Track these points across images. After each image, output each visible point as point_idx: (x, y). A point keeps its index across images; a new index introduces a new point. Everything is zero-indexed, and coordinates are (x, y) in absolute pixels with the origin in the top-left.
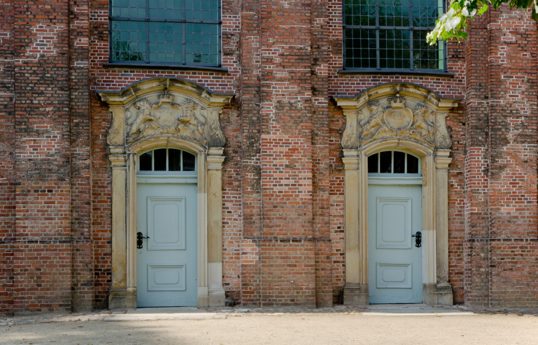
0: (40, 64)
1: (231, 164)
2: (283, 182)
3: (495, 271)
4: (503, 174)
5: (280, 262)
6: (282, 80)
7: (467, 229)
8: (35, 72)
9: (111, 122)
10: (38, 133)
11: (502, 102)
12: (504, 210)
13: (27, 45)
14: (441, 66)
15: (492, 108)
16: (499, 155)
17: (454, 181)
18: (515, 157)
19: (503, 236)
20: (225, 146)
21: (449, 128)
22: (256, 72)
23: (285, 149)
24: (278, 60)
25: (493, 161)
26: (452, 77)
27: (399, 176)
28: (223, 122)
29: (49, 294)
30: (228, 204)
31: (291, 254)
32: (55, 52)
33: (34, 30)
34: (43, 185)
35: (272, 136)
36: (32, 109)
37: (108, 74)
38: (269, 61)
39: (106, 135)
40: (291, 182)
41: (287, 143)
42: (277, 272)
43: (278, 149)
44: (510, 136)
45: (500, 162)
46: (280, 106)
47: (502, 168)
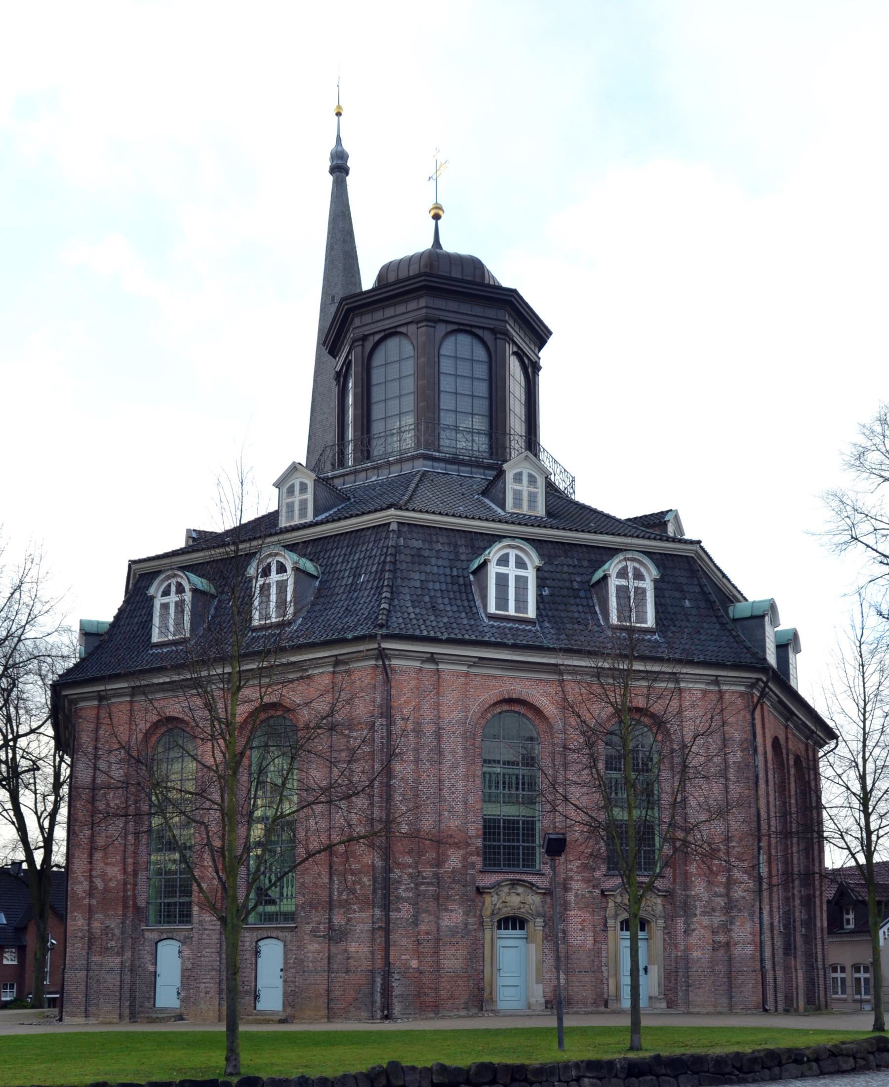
0: (453, 872)
1: (547, 927)
2: (579, 938)
3: (690, 989)
4: (694, 934)
5: (577, 984)
6: (578, 881)
7: (674, 965)
8: (450, 877)
9: (484, 903)
10: (451, 911)
11: (693, 893)
12: (695, 954)
13: (446, 861)
14: (537, 868)
15: (687, 896)
16: (692, 923)
17: (666, 937)
18: (700, 924)
19: (694, 970)
20: (544, 916)
21: (663, 906)
22: (563, 876)
23: (579, 920)
24: (575, 870)
25: (689, 926)
26: (543, 874)
27: (514, 932)
28: (544, 902)
29: (457, 1002)
30: (546, 950)
31: (584, 980)
32: (460, 865)
33: (449, 853)
34: (454, 940)
35: (572, 912)
36: (448, 897)
37: (482, 876)
38: (571, 870)
39: (481, 910)
40: (583, 938)
41: (580, 916)
42: (576, 990)
43: (576, 920)
44: (698, 912)
45: (692, 927)
46: (576, 896)
47: (693, 930)
